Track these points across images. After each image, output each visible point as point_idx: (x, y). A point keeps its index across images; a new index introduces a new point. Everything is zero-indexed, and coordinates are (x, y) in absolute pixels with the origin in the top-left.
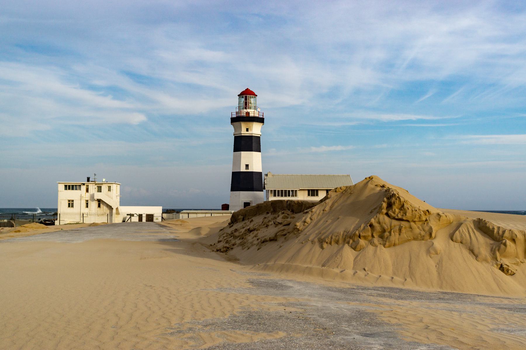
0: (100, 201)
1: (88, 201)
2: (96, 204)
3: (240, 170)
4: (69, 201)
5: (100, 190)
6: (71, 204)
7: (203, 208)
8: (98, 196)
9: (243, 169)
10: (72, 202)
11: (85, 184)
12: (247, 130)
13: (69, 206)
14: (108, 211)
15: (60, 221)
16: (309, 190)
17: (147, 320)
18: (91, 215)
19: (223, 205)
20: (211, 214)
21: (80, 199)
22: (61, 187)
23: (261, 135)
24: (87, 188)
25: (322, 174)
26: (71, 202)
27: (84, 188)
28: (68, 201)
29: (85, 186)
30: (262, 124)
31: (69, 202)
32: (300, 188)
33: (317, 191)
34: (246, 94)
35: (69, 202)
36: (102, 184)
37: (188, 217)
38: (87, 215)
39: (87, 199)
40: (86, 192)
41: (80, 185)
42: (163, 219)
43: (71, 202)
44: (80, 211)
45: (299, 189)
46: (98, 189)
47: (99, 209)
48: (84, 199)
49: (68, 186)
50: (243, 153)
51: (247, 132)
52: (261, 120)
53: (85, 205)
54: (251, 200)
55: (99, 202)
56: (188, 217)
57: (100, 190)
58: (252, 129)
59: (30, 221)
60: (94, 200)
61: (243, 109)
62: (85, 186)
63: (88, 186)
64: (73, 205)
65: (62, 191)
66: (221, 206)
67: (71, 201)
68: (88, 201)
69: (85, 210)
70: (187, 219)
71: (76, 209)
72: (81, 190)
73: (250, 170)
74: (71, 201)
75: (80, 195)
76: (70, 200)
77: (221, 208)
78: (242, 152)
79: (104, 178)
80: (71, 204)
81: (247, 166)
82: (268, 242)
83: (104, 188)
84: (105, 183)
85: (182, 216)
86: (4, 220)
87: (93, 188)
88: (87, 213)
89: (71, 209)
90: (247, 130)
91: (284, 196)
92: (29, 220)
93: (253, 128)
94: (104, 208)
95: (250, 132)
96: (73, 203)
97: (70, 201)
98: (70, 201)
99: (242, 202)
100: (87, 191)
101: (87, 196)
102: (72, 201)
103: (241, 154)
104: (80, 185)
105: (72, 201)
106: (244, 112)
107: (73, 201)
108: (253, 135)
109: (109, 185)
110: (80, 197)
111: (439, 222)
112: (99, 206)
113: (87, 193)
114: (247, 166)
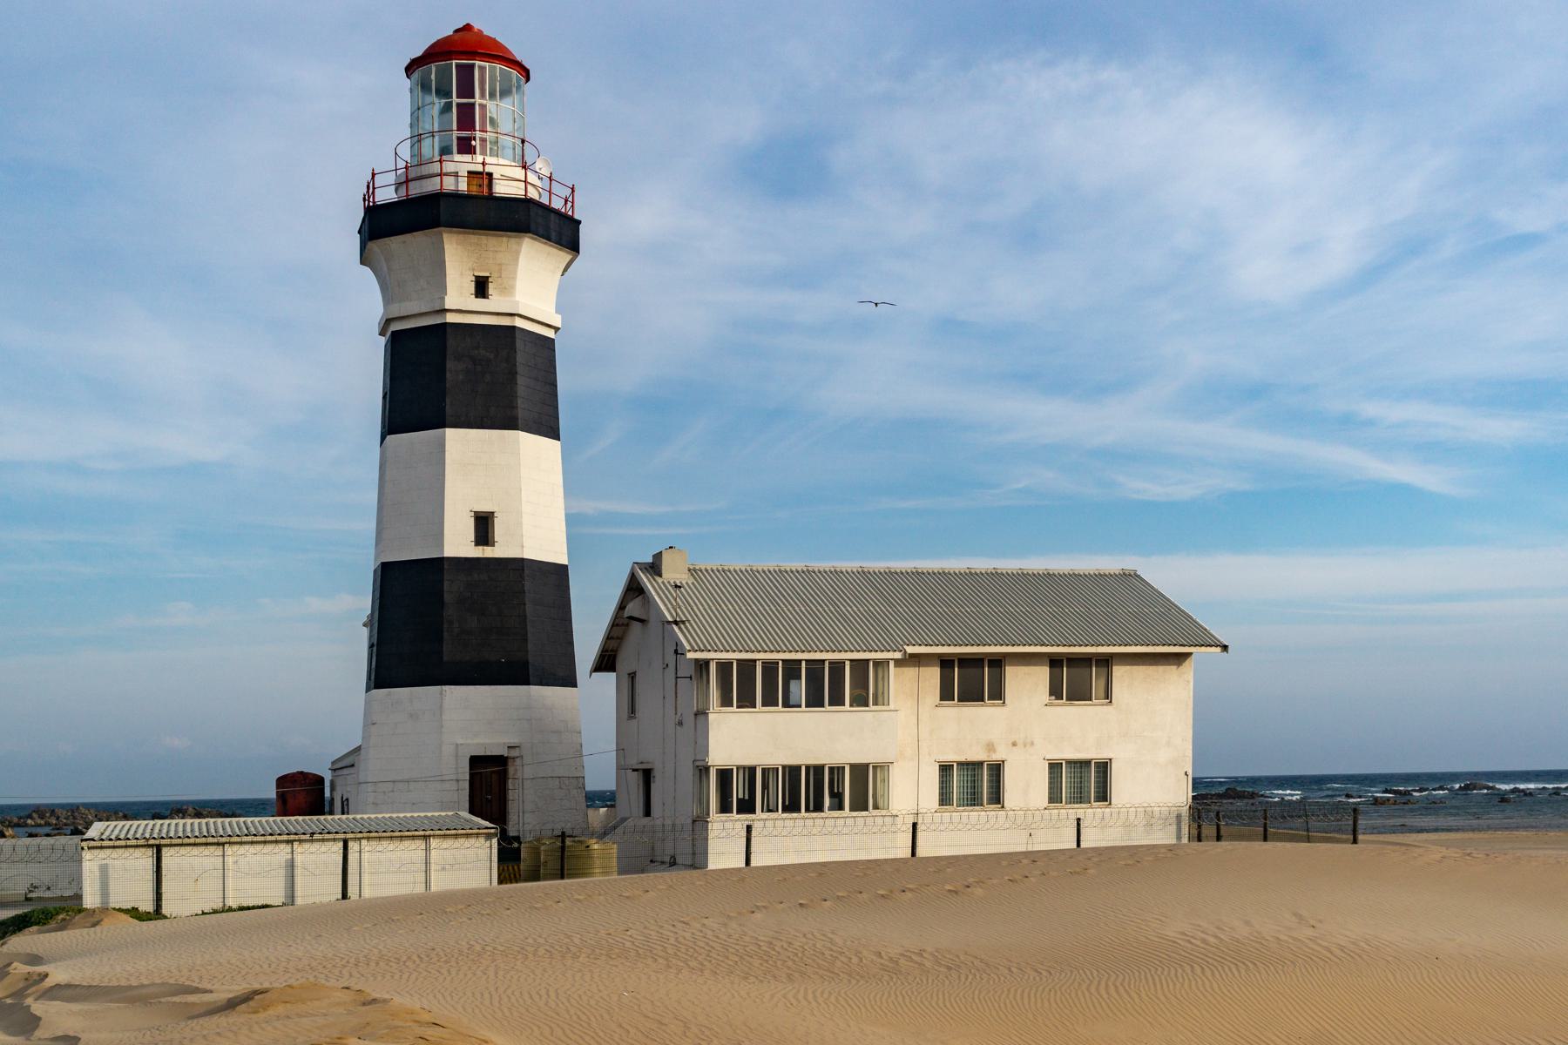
3: (443, 553)
9: (459, 543)
12: (481, 288)
16: (946, 663)
19: (282, 781)
23: (557, 329)
30: (565, 257)
32: (910, 650)
33: (998, 662)
37: (1078, 845)
45: (898, 655)
50: (458, 441)
51: (481, 304)
54: (514, 740)
56: (1078, 845)
58: (513, 287)
61: (445, 151)
70: (740, 869)
73: (498, 551)
77: (271, 793)
81: (484, 526)
85: (104, 870)
90: (481, 288)
91: (764, 705)
93: (514, 278)
95: (495, 302)
106: (457, 173)
108: (519, 323)
111: (1002, 813)
114: (484, 526)
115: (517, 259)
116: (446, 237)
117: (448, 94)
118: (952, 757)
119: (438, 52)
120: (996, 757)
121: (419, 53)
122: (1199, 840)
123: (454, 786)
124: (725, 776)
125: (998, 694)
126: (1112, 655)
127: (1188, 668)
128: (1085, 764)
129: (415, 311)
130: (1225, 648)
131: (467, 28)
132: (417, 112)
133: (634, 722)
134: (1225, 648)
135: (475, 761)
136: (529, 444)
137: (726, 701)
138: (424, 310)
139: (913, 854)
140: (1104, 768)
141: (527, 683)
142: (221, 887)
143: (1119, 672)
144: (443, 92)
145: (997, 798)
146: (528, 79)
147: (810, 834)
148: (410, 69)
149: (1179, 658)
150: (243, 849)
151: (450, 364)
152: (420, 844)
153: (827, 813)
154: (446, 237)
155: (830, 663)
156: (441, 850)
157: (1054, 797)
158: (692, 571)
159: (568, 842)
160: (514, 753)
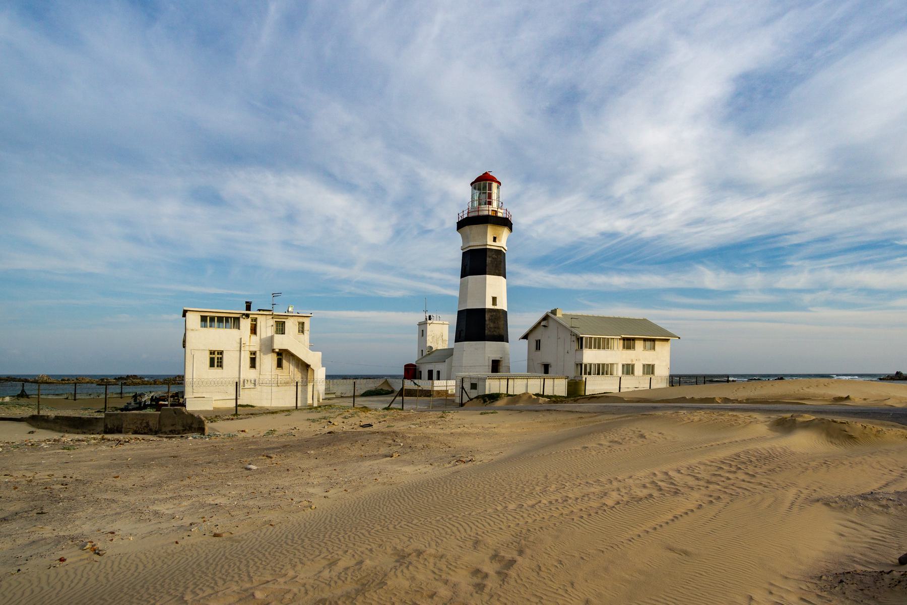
0: (283, 356)
1: (254, 353)
2: (271, 360)
4: (211, 354)
5: (281, 328)
6: (216, 360)
7: (238, 371)
8: (281, 342)
9: (489, 305)
10: (220, 356)
11: (251, 316)
12: (495, 239)
13: (212, 365)
14: (298, 376)
15: (235, 398)
18: (261, 384)
20: (508, 379)
21: (238, 349)
22: (193, 320)
27: (246, 324)
28: (208, 353)
34: (483, 183)
36: (285, 317)
38: (255, 384)
39: (253, 349)
40: (251, 333)
41: (238, 318)
43: (216, 356)
45: (620, 337)
46: (277, 329)
47: (279, 370)
48: (247, 348)
49: (216, 318)
54: (501, 356)
55: (280, 357)
56: (620, 391)
57: (281, 328)
59: (67, 398)
60: (273, 351)
63: (256, 320)
64: (221, 362)
65: (197, 330)
67: (216, 353)
68: (254, 353)
69: (248, 374)
71: (229, 370)
72: (239, 329)
74: (216, 353)
75: (239, 341)
76: (214, 351)
80: (216, 360)
81: (494, 299)
83: (291, 325)
84: (292, 316)
85: (490, 384)
86: (4, 397)
87: (266, 327)
88: (255, 381)
89: (216, 372)
90: (495, 239)
92: (65, 396)
93: (502, 237)
94: (290, 371)
96: (221, 358)
97: (214, 354)
98: (214, 354)
100: (254, 331)
101: (254, 343)
102: (218, 354)
103: (484, 282)
104: (238, 318)
105: (218, 354)
107: (221, 353)
109: (301, 320)
111: (634, 377)
112: (280, 365)
113: (253, 337)
115: (503, 233)
116: (489, 226)
117: (481, 190)
119: (479, 179)
122: (673, 386)
124: (586, 365)
126: (635, 338)
127: (669, 341)
129: (476, 244)
130: (679, 338)
133: (538, 353)
134: (679, 338)
135: (493, 361)
136: (502, 278)
138: (481, 244)
139: (650, 388)
140: (653, 366)
141: (503, 341)
142: (807, 379)
144: (479, 189)
145: (633, 373)
146: (500, 185)
147: (615, 380)
148: (471, 184)
150: (519, 380)
151: (488, 259)
152: (552, 380)
153: (592, 375)
154: (489, 226)
156: (531, 382)
157: (644, 373)
159: (73, 398)
160: (502, 359)
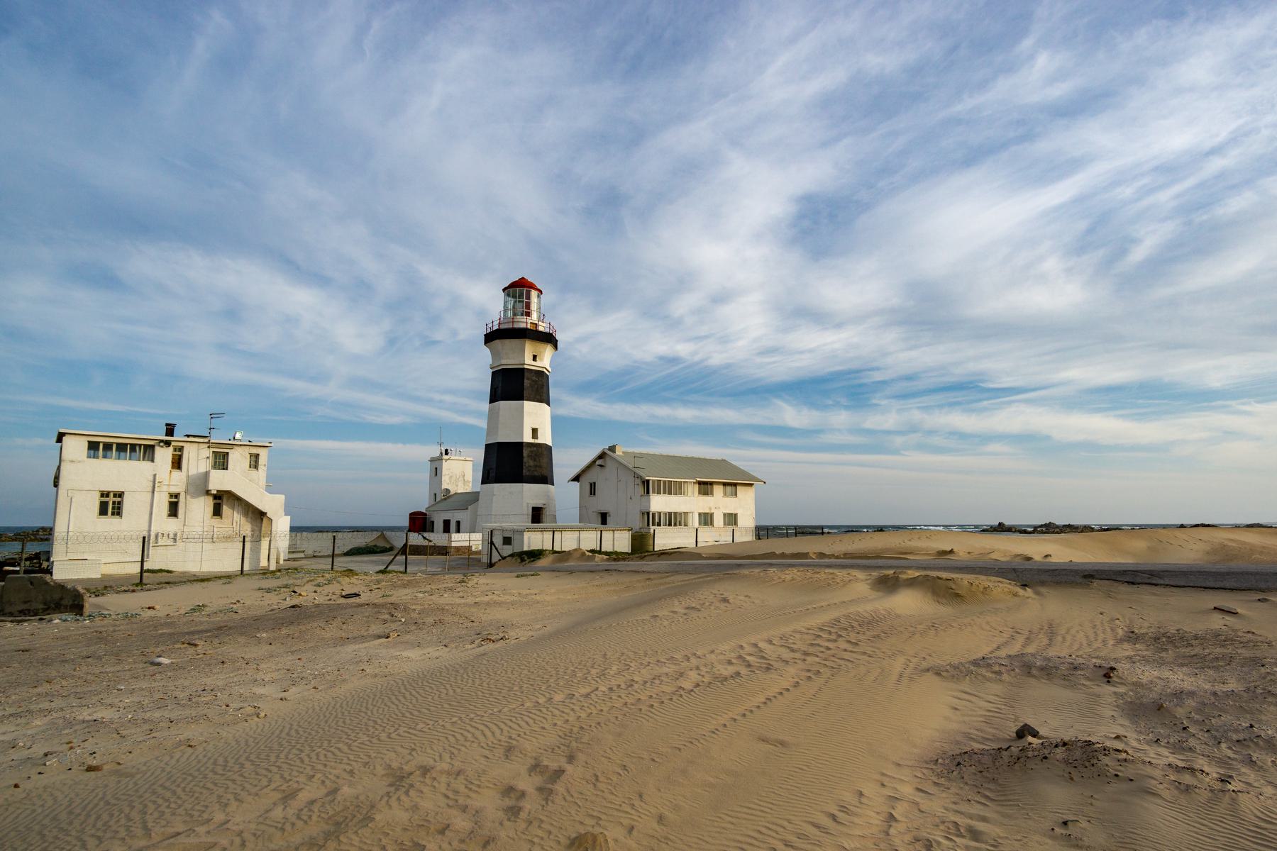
0: (221, 500)
2: (206, 504)
8: (219, 481)
9: (527, 438)
11: (173, 444)
12: (535, 358)
13: (103, 511)
14: (246, 528)
15: (140, 560)
17: (390, 803)
18: (187, 539)
20: (554, 532)
21: (150, 489)
22: (75, 448)
24: (177, 458)
25: (689, 456)
26: (111, 499)
28: (98, 494)
29: (171, 449)
31: (105, 499)
35: (105, 499)
36: (230, 447)
37: (697, 545)
39: (174, 490)
40: (172, 468)
41: (153, 447)
42: (493, 547)
44: (147, 528)
45: (695, 481)
47: (216, 521)
48: (165, 489)
51: (534, 363)
52: (549, 339)
53: (165, 508)
54: (544, 502)
55: (218, 501)
56: (697, 545)
57: (221, 461)
60: (208, 492)
62: (171, 449)
63: (181, 449)
64: (119, 508)
66: (408, 515)
67: (112, 495)
69: (163, 524)
71: (133, 520)
72: (153, 461)
73: (539, 441)
74: (112, 495)
75: (151, 478)
77: (406, 523)
78: (526, 402)
79: (240, 430)
80: (111, 504)
82: (238, 578)
83: (238, 458)
84: (241, 445)
85: (529, 538)
87: (197, 459)
89: (110, 523)
90: (535, 358)
94: (234, 520)
96: (119, 503)
99: (528, 507)
100: (177, 463)
101: (176, 482)
103: (523, 403)
104: (153, 447)
107: (121, 495)
110: (151, 484)
112: (217, 512)
113: (176, 473)
118: (702, 511)
119: (513, 285)
120: (712, 511)
121: (507, 286)
122: (759, 539)
123: (526, 516)
125: (712, 494)
128: (732, 514)
131: (523, 278)
132: (505, 303)
137: (654, 492)
140: (736, 515)
143: (739, 488)
145: (712, 524)
148: (504, 290)
149: (751, 485)
151: (525, 381)
152: (611, 532)
153: (673, 527)
155: (104, 445)
156: (584, 535)
158: (623, 452)
